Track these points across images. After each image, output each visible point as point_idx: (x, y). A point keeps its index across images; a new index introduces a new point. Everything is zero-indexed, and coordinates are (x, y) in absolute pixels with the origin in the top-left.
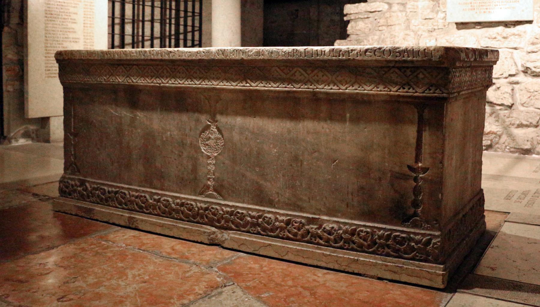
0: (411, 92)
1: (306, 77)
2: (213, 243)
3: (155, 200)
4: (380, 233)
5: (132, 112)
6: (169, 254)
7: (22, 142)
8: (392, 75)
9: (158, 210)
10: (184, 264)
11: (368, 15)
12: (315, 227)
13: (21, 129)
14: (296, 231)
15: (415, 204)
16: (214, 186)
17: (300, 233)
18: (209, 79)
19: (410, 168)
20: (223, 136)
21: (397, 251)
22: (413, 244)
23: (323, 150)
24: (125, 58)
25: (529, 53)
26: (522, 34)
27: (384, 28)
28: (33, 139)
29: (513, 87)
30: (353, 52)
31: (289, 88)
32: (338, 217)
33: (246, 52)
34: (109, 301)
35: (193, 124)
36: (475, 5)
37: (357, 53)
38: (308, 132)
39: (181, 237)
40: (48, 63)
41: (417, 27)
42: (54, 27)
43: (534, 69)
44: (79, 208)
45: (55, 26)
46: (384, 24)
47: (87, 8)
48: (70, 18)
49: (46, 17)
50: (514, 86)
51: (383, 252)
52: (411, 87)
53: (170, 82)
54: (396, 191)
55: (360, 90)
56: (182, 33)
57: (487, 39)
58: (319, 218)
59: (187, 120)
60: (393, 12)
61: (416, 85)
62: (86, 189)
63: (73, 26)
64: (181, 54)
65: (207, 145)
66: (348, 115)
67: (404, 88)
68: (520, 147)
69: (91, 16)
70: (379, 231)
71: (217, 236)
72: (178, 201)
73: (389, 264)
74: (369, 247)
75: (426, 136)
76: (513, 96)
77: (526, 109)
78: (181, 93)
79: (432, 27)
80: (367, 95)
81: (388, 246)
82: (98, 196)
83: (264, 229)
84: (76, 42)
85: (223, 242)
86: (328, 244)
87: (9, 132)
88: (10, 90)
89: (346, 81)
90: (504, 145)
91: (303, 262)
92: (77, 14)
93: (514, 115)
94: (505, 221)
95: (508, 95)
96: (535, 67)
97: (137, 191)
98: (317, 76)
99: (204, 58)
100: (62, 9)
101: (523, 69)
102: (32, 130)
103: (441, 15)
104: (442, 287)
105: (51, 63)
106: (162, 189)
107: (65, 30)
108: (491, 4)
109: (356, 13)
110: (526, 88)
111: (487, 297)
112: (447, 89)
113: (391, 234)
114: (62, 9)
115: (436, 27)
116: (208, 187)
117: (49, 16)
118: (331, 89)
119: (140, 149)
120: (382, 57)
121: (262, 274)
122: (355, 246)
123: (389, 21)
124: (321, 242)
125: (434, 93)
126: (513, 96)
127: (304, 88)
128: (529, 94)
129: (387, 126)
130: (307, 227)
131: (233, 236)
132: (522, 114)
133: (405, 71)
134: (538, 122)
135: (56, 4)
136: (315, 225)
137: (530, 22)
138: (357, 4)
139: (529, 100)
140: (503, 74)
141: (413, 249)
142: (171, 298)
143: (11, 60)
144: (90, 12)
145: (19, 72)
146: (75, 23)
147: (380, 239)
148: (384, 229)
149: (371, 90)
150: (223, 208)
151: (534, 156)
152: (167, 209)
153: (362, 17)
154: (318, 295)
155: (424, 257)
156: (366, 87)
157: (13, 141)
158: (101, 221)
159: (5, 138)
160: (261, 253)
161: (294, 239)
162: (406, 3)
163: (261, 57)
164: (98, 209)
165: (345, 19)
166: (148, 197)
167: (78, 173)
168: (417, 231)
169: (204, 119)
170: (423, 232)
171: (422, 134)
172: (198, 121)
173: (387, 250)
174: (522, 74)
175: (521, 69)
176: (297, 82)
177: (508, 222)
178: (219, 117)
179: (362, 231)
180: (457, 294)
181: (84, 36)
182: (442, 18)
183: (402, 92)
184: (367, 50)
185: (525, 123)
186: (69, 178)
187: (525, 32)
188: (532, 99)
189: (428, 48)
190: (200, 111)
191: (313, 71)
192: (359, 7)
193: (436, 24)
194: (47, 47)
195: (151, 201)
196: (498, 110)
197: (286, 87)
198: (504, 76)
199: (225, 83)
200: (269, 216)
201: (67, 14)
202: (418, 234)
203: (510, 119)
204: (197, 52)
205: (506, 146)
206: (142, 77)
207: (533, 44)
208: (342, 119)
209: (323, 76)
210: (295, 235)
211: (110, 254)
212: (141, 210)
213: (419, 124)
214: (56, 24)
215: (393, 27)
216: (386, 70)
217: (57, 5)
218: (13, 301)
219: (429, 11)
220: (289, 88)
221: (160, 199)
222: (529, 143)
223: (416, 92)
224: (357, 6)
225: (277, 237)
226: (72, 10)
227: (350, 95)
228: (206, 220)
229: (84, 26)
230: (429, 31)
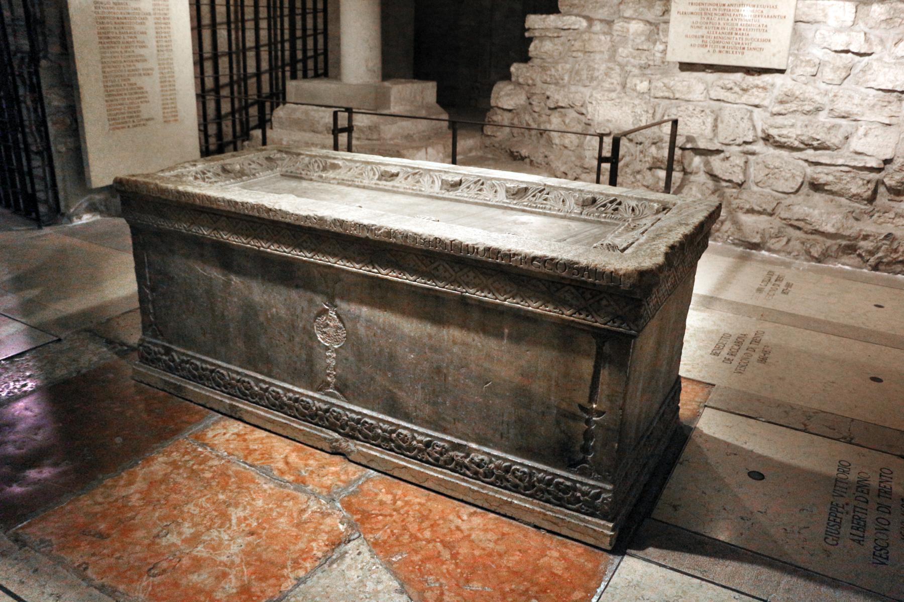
0: (590, 321)
1: (452, 275)
2: (336, 452)
3: (261, 389)
4: (540, 475)
5: (224, 275)
6: (282, 473)
7: (88, 219)
8: (566, 295)
9: (266, 401)
10: (300, 494)
11: (558, 33)
12: (462, 455)
13: (84, 202)
14: (437, 455)
15: (585, 450)
16: (335, 384)
17: (442, 458)
18: (325, 253)
19: (582, 408)
20: (344, 326)
21: (559, 499)
22: (579, 494)
23: (473, 366)
24: (210, 206)
25: (775, 115)
26: (768, 87)
27: (580, 54)
28: (101, 213)
29: (747, 159)
30: (516, 257)
31: (429, 285)
32: (489, 447)
33: (372, 230)
34: (209, 573)
35: (305, 304)
36: (708, 40)
37: (521, 259)
38: (455, 343)
39: (297, 439)
40: (111, 110)
41: (625, 60)
42: (115, 57)
43: (777, 138)
44: (166, 382)
45: (116, 54)
46: (581, 49)
47: (159, 23)
48: (135, 40)
49: (101, 43)
50: (750, 157)
51: (543, 497)
52: (591, 314)
53: (272, 247)
54: (563, 432)
55: (521, 305)
56: (299, 38)
57: (719, 89)
58: (466, 446)
59: (297, 298)
60: (594, 33)
61: (596, 312)
62: (173, 361)
63: (142, 51)
64: (284, 215)
65: (325, 333)
66: (506, 331)
67: (580, 314)
68: (747, 240)
69: (167, 35)
70: (540, 473)
71: (340, 445)
72: (291, 395)
73: (548, 513)
74: (526, 489)
75: (604, 374)
76: (745, 171)
77: (760, 189)
78: (289, 263)
79: (646, 61)
80: (532, 312)
81: (549, 492)
82: (190, 371)
83: (399, 447)
84: (149, 74)
85: (349, 453)
86: (476, 476)
87: (68, 207)
88: (61, 150)
89: (505, 291)
90: (727, 234)
91: (445, 492)
92: (145, 33)
93: (745, 196)
94: (706, 406)
95: (739, 168)
96: (779, 136)
97: (238, 373)
98: (468, 276)
99: (317, 226)
100: (123, 28)
101: (763, 136)
102: (100, 200)
103: (659, 47)
104: (609, 548)
105: (115, 109)
106: (270, 376)
107: (130, 59)
108: (731, 41)
109: (542, 29)
110: (764, 162)
111: (660, 565)
112: (637, 326)
113: (553, 479)
114: (123, 28)
115: (651, 63)
116: (328, 384)
117: (106, 41)
118: (485, 297)
119: (238, 322)
120: (554, 271)
121: (396, 516)
122: (509, 485)
123: (587, 46)
124: (468, 472)
125: (619, 327)
126: (745, 171)
127: (449, 289)
128: (767, 171)
129: (555, 353)
130: (451, 453)
131: (360, 448)
132: (755, 196)
133: (583, 293)
134: (773, 210)
135: (113, 22)
136: (461, 452)
137: (782, 71)
138: (544, 16)
139: (766, 178)
140: (735, 140)
141: (578, 500)
142: (284, 567)
143: (58, 107)
144: (165, 28)
145: (72, 124)
146: (144, 47)
147: (539, 483)
148: (545, 472)
149: (538, 308)
150: (348, 413)
151: (763, 252)
152: (277, 402)
153: (550, 35)
154: (461, 558)
155: (591, 510)
156: (531, 303)
157: (75, 219)
158: (195, 403)
159: (63, 215)
160: (395, 475)
161: (436, 463)
162: (613, 21)
163: (392, 240)
164: (192, 388)
165: (527, 34)
166: (252, 383)
167: (160, 337)
168: (585, 480)
169: (320, 301)
170: (591, 482)
171: (600, 371)
172: (311, 301)
173: (546, 496)
174: (761, 142)
175: (760, 134)
176: (441, 280)
177: (709, 407)
178: (338, 302)
179: (518, 470)
180: (626, 558)
181: (159, 64)
182: (661, 50)
183: (576, 318)
184: (534, 258)
185: (757, 208)
186: (149, 342)
187: (772, 85)
188: (769, 178)
189: (616, 270)
190: (314, 290)
191: (461, 270)
192: (548, 19)
193: (652, 58)
194: (107, 86)
195: (256, 389)
196: (723, 187)
197: (425, 283)
198: (737, 142)
199: (345, 262)
200: (405, 432)
201: (131, 35)
202: (586, 484)
203: (737, 201)
204: (306, 217)
205: (729, 236)
206: (236, 234)
207: (781, 102)
208: (499, 335)
209: (474, 278)
210: (437, 460)
211: (208, 475)
212: (244, 396)
213: (597, 358)
214: (117, 52)
215: (592, 55)
216: (559, 286)
217: (115, 23)
218: (94, 577)
219: (643, 38)
220: (429, 285)
221: (267, 389)
222: (759, 236)
223: (596, 322)
224: (545, 18)
225: (414, 458)
226: (138, 28)
227: (510, 309)
228: (327, 423)
229: (158, 51)
230: (641, 67)
